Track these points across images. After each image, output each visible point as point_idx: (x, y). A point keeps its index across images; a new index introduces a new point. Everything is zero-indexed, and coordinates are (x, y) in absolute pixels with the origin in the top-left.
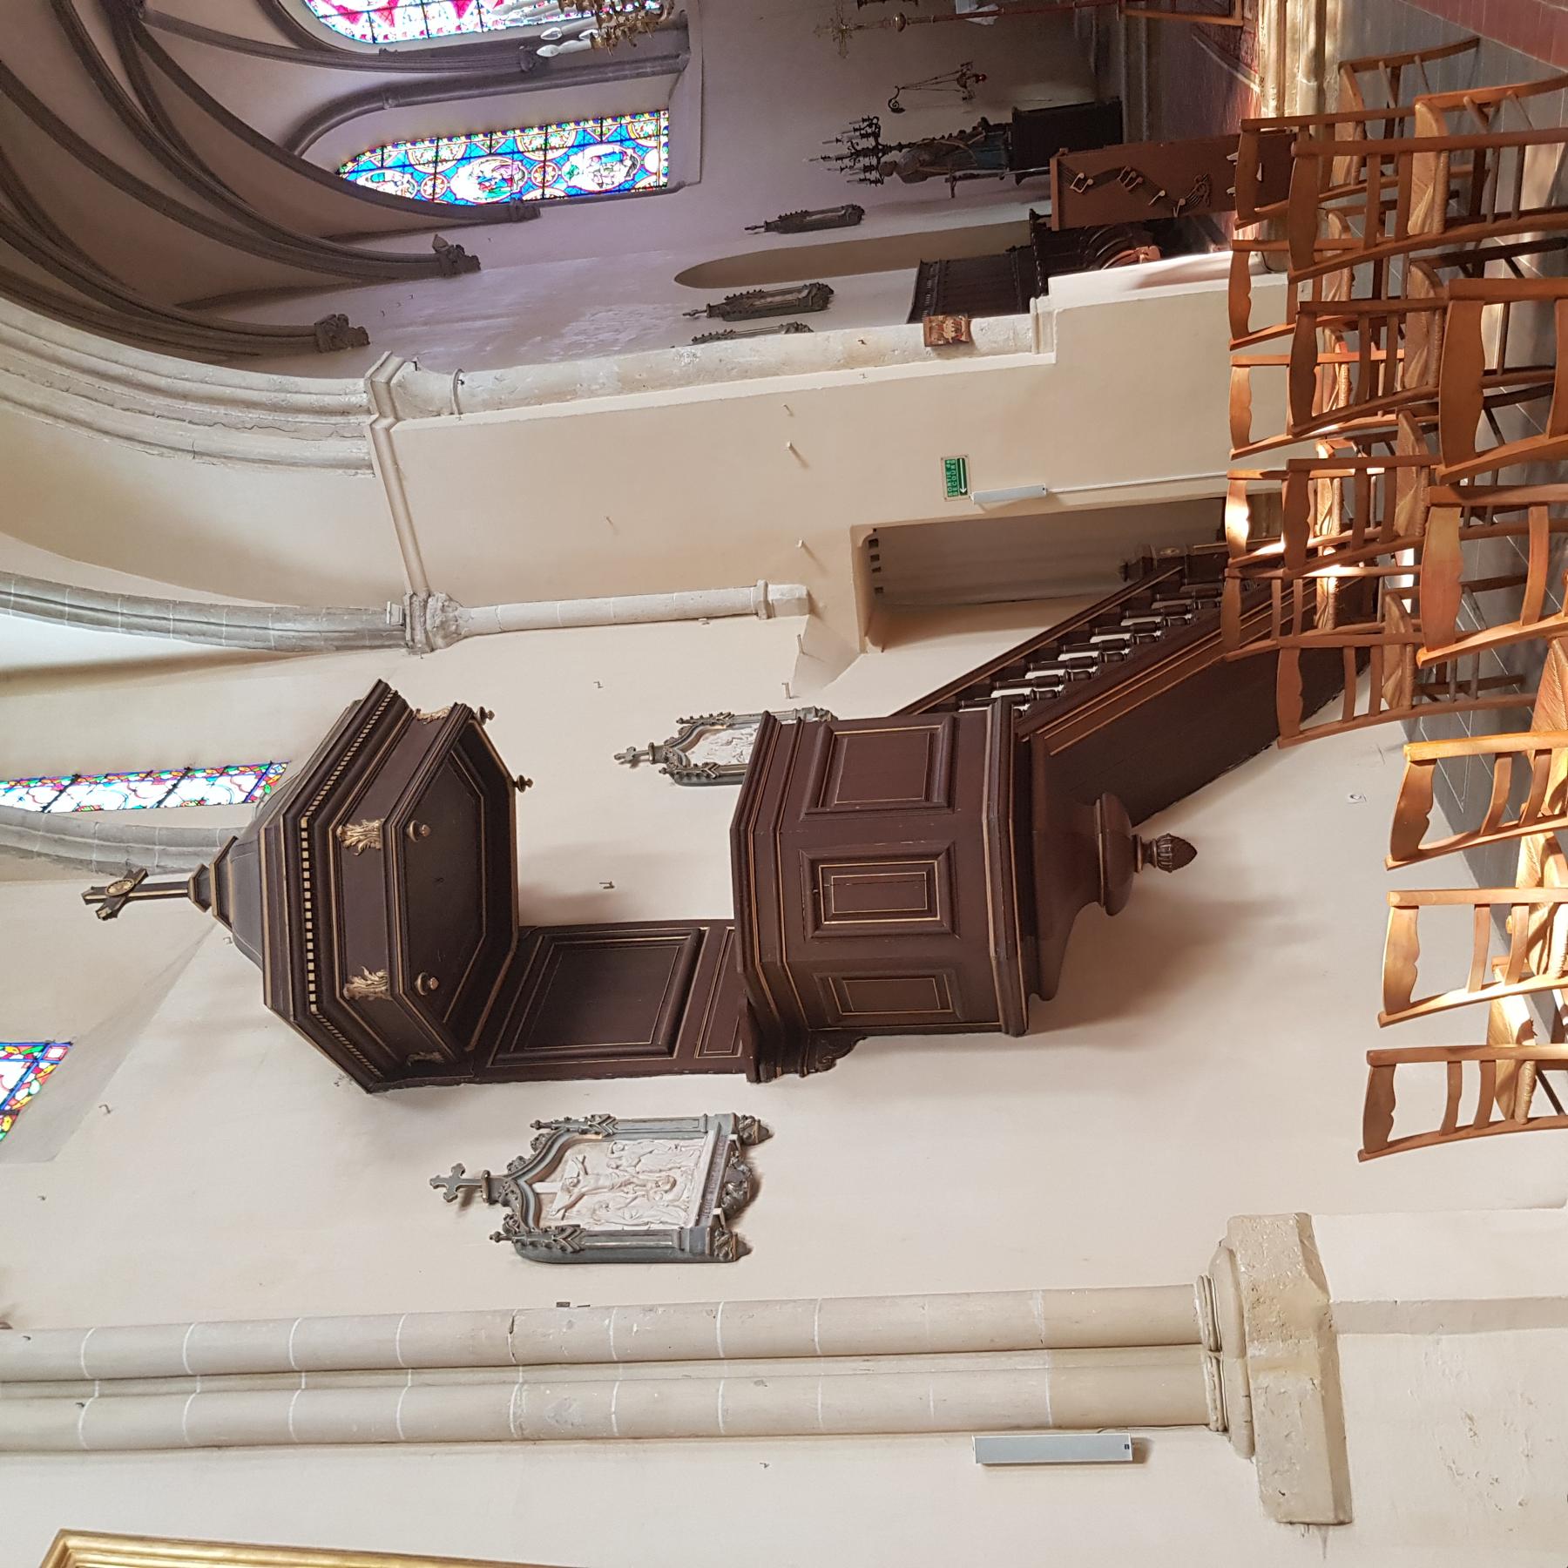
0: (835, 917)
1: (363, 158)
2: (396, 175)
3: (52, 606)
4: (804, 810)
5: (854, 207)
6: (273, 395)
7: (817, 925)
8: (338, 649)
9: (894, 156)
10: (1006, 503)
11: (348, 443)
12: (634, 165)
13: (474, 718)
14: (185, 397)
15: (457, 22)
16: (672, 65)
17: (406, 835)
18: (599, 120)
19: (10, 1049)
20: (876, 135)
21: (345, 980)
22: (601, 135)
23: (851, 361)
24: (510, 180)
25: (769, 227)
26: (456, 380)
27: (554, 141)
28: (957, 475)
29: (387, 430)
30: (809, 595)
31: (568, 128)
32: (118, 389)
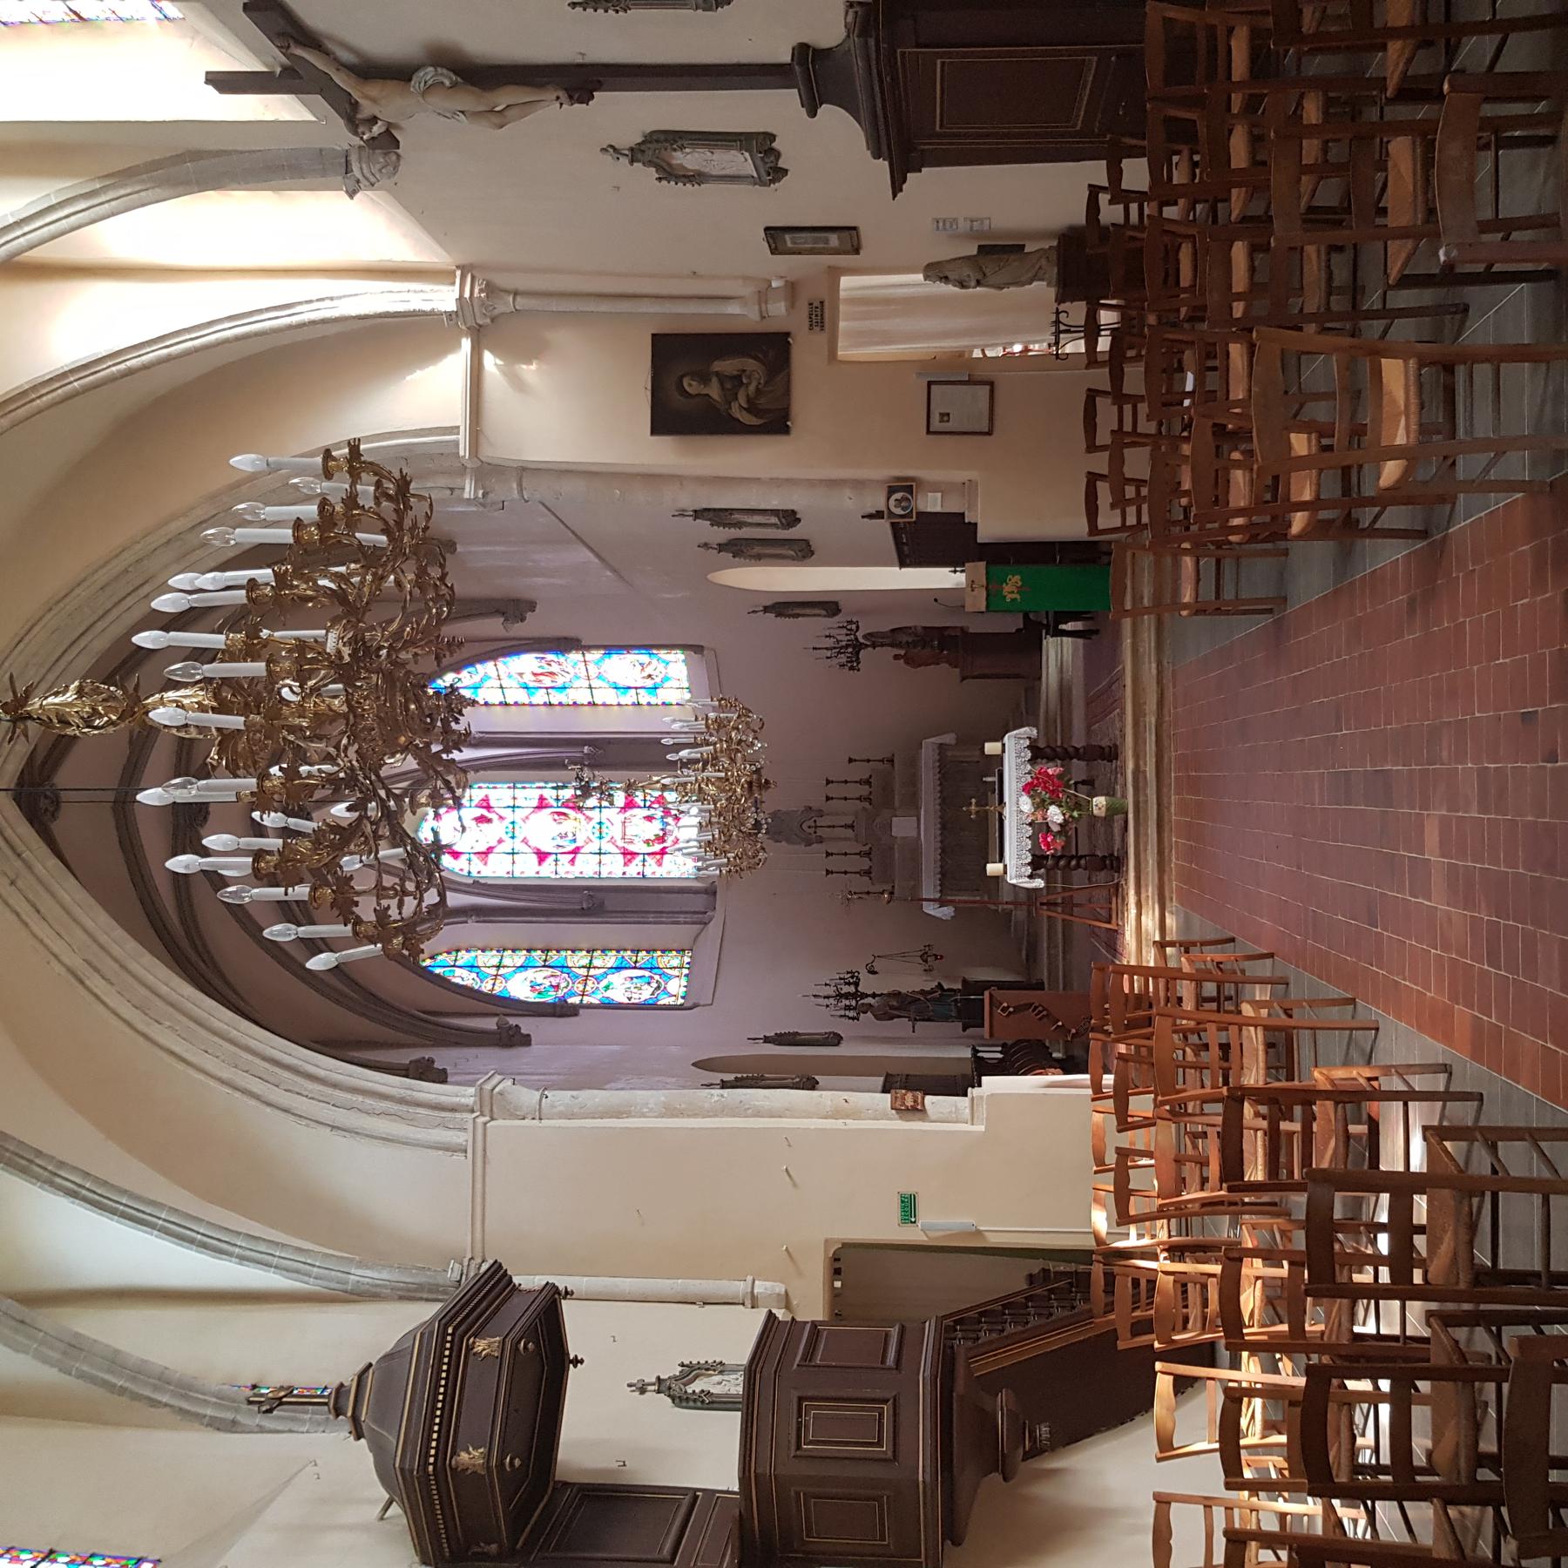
0: (811, 1443)
1: (440, 957)
2: (464, 973)
3: (188, 1232)
4: (797, 1362)
5: (835, 1034)
6: (402, 1091)
7: (799, 1447)
8: (401, 1298)
9: (869, 1000)
10: (943, 1233)
11: (451, 1133)
12: (658, 988)
13: (559, 1294)
14: (335, 1086)
15: (537, 868)
16: (701, 919)
17: (517, 1349)
18: (636, 951)
19: (109, 1560)
20: (857, 984)
21: (454, 1453)
22: (636, 962)
23: (836, 1114)
24: (557, 987)
25: (767, 1040)
26: (542, 1094)
27: (596, 963)
28: (909, 1207)
29: (485, 1124)
30: (786, 1292)
31: (610, 953)
32: (286, 1074)
